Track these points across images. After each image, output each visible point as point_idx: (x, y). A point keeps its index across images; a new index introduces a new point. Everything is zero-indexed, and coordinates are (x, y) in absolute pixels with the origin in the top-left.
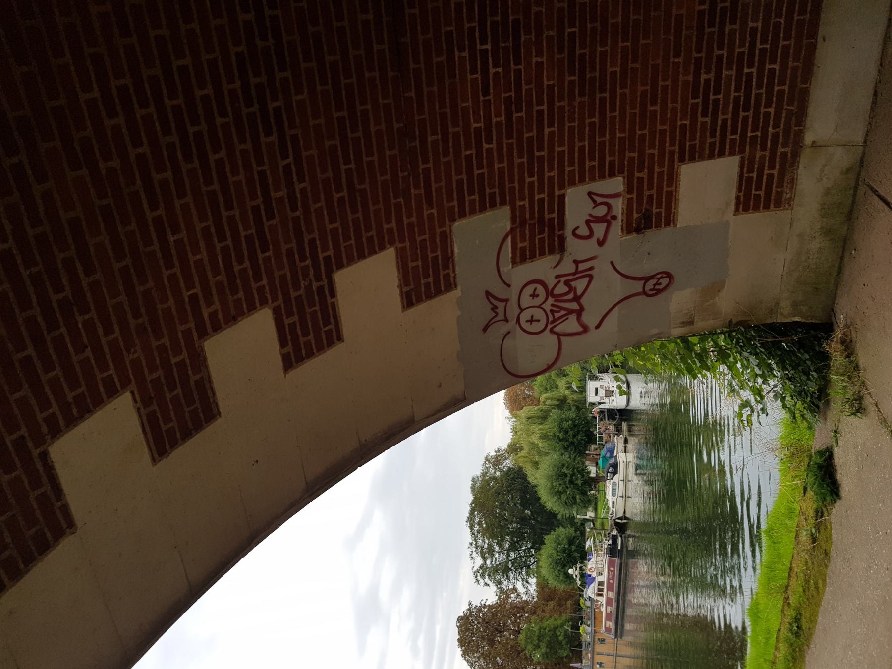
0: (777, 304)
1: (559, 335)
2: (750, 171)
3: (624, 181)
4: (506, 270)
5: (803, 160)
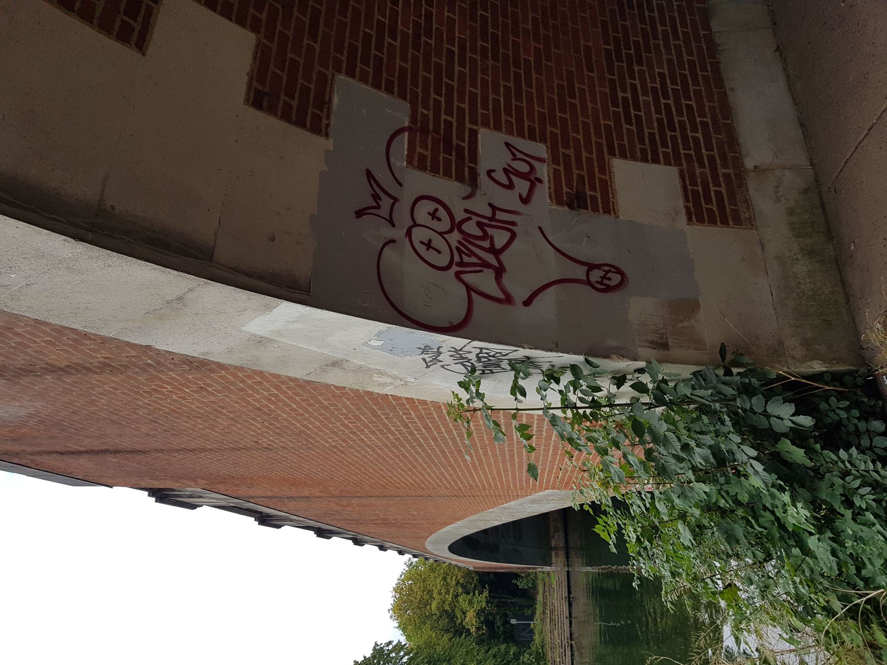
0: (781, 343)
1: (469, 288)
2: (694, 183)
3: (547, 150)
4: (398, 164)
5: (752, 183)
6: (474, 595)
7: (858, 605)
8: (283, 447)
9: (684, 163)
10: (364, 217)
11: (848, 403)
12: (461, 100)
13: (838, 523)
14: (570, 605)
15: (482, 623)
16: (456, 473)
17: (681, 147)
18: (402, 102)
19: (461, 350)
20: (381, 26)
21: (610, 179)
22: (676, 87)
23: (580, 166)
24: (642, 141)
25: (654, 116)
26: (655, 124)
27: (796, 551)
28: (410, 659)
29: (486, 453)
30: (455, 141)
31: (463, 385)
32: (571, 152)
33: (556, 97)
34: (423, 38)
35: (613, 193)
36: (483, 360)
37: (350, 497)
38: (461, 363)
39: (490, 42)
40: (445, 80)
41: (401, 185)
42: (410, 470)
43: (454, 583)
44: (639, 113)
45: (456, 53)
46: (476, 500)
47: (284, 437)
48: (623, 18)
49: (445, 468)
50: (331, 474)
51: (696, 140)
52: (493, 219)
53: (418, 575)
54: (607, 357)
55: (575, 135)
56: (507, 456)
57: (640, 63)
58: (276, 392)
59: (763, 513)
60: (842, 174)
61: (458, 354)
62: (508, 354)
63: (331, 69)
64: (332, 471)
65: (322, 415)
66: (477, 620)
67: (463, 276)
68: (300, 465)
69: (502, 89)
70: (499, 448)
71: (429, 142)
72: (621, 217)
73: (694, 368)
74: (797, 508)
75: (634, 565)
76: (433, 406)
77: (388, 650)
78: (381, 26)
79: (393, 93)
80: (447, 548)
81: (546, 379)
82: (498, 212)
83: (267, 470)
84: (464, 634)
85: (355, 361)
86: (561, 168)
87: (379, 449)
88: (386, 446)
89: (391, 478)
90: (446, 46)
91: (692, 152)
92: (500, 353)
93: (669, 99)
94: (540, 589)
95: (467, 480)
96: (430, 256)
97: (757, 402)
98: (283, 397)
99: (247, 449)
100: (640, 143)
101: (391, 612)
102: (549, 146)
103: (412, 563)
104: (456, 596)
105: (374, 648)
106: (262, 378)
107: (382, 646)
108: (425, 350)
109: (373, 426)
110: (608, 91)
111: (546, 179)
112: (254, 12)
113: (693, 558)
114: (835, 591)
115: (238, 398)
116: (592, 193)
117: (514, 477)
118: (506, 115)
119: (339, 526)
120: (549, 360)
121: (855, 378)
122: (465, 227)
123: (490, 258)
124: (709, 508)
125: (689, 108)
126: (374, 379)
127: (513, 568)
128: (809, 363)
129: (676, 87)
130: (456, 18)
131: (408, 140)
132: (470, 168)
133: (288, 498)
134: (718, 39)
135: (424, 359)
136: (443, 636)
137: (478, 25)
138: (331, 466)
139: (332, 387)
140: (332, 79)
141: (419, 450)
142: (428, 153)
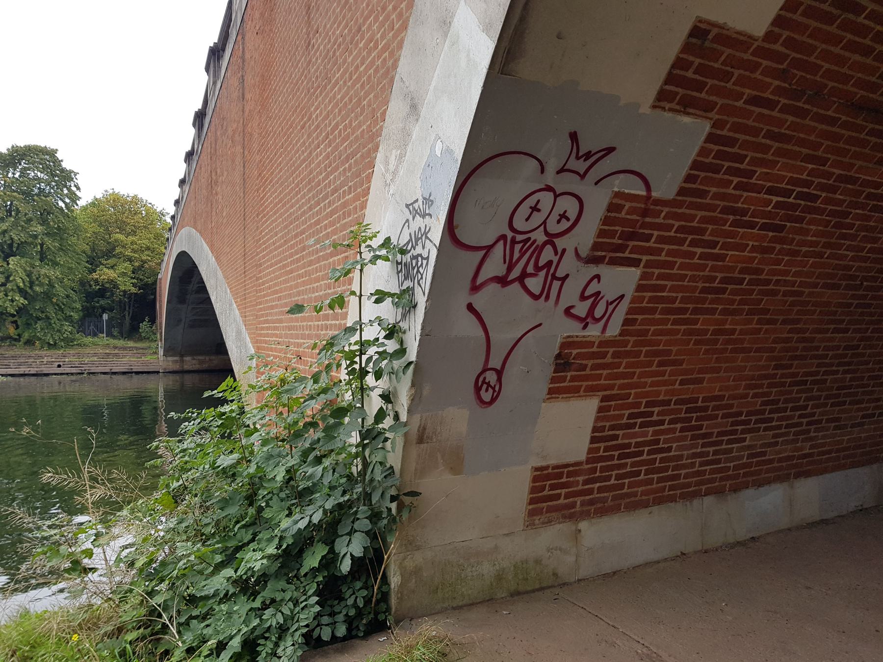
0: (418, 548)
1: (489, 248)
4: (617, 182)
6: (132, 278)
7: (160, 616)
8: (310, 61)
9: (589, 466)
10: (570, 141)
11: (361, 606)
12: (670, 253)
13: (243, 598)
14: (124, 373)
15: (103, 285)
16: (276, 249)
17: (604, 464)
18: (675, 190)
19: (427, 238)
20: (750, 174)
21: (580, 396)
22: (658, 462)
23: (595, 367)
24: (612, 428)
25: (633, 441)
26: (627, 441)
27: (218, 558)
28: (61, 209)
29: (300, 276)
30: (632, 244)
31: (387, 242)
32: (609, 359)
33: (661, 347)
34: (731, 217)
35: (567, 398)
36: (414, 262)
37: (243, 144)
38: (411, 239)
39: (719, 285)
40: (690, 237)
41: (596, 184)
42: (280, 201)
43: (144, 258)
44: (637, 427)
45: (713, 251)
46: (241, 275)
47: (322, 62)
48: (725, 416)
49: (282, 237)
50: (276, 117)
51: (608, 478)
52: (554, 277)
53: (152, 221)
54: (413, 385)
55: (623, 365)
56: (296, 298)
57: (682, 430)
58: (380, 47)
59: (251, 532)
60: (572, 605)
61: (422, 236)
62: (421, 286)
63: (717, 117)
64: (279, 118)
65: (351, 100)
66: (106, 281)
67: (501, 243)
68: (287, 83)
69: (674, 295)
70: (307, 289)
71: (634, 217)
72: (544, 404)
73: (397, 468)
74: (261, 559)
75: (193, 413)
76: (359, 216)
77: (70, 186)
78: (750, 174)
79: (684, 182)
80: (184, 250)
81: (390, 326)
82: (559, 283)
83: (281, 47)
84: (90, 266)
85: (417, 128)
86: (595, 349)
87: (306, 165)
88: (311, 172)
89: (271, 182)
90: (722, 240)
91: (598, 474)
92: (422, 278)
93: (647, 455)
94: (139, 345)
95: (268, 261)
96: (524, 210)
97: (364, 524)
98: (373, 55)
99: (309, 23)
100: (610, 426)
101: (111, 191)
102: (617, 339)
103: (164, 216)
104: (130, 260)
105: (71, 172)
106: (399, 29)
107: (75, 180)
108: (428, 201)
109: (335, 156)
110: (661, 398)
111: (586, 333)
112: (784, 37)
113: (204, 468)
114: (172, 599)
115: (373, 6)
116: (568, 378)
117: (272, 307)
118: (650, 297)
119: (209, 134)
120: (412, 328)
121: (384, 612)
122: (549, 248)
123: (516, 273)
124: (256, 483)
125: (638, 473)
126: (394, 151)
127: (161, 318)
128: (398, 573)
129: (658, 462)
130: (746, 253)
131: (638, 195)
132: (605, 257)
133: (243, 76)
134: (696, 502)
135: (417, 201)
136: (87, 244)
137: (736, 275)
138: (286, 116)
139: (386, 107)
140: (707, 118)
141: (306, 208)
142: (623, 215)
